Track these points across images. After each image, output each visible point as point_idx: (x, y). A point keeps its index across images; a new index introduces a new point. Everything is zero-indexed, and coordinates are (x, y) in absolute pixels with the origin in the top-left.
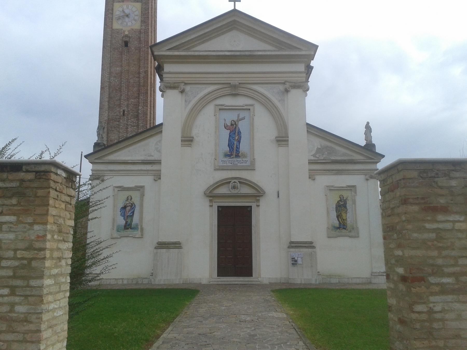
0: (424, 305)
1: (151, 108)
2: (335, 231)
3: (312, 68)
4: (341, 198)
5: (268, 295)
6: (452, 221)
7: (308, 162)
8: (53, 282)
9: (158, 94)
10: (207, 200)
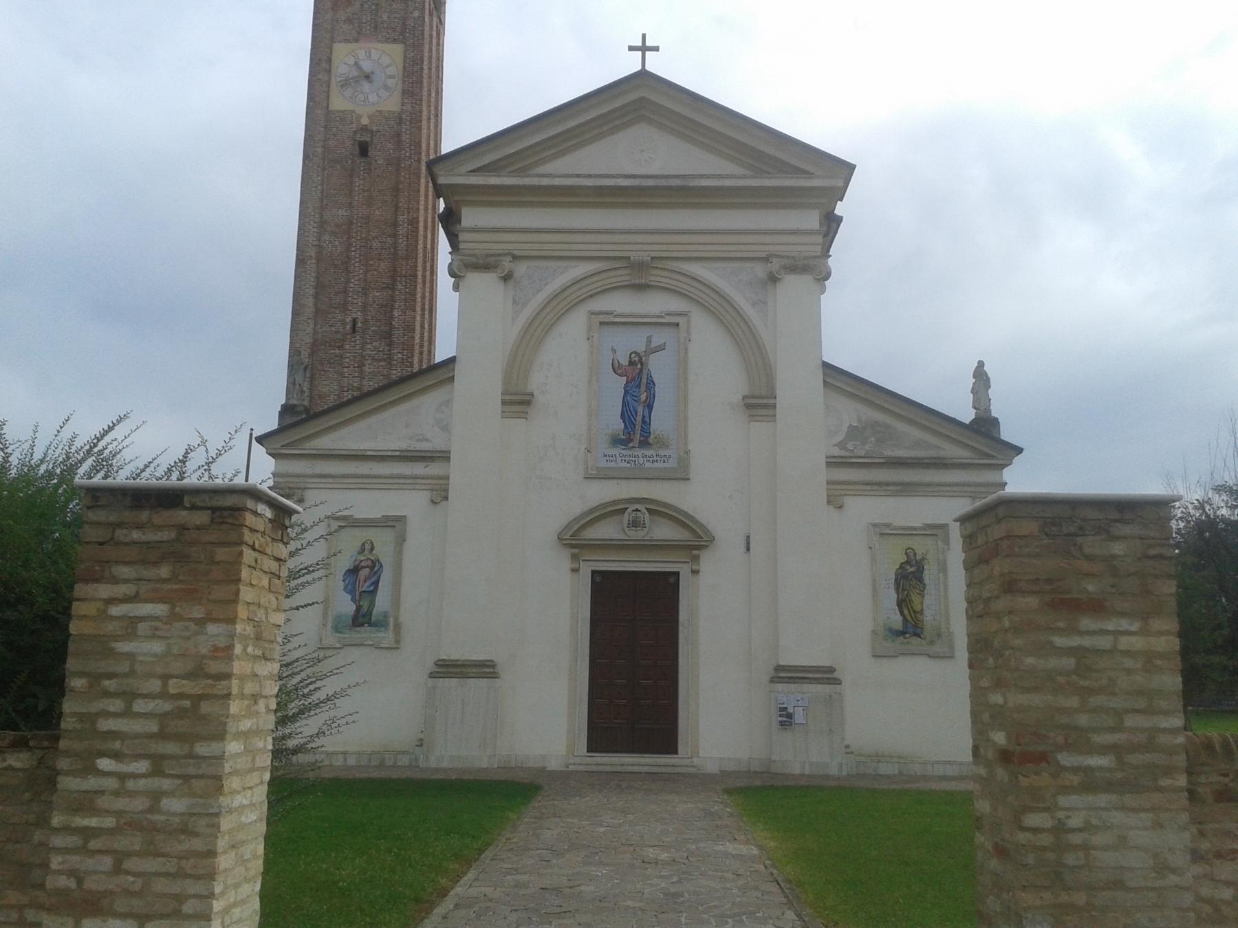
0: (1047, 814)
1: (423, 315)
2: (893, 641)
3: (839, 220)
4: (910, 551)
5: (716, 802)
6: (1113, 631)
7: (827, 462)
8: (242, 747)
9: (444, 281)
10: (566, 553)
